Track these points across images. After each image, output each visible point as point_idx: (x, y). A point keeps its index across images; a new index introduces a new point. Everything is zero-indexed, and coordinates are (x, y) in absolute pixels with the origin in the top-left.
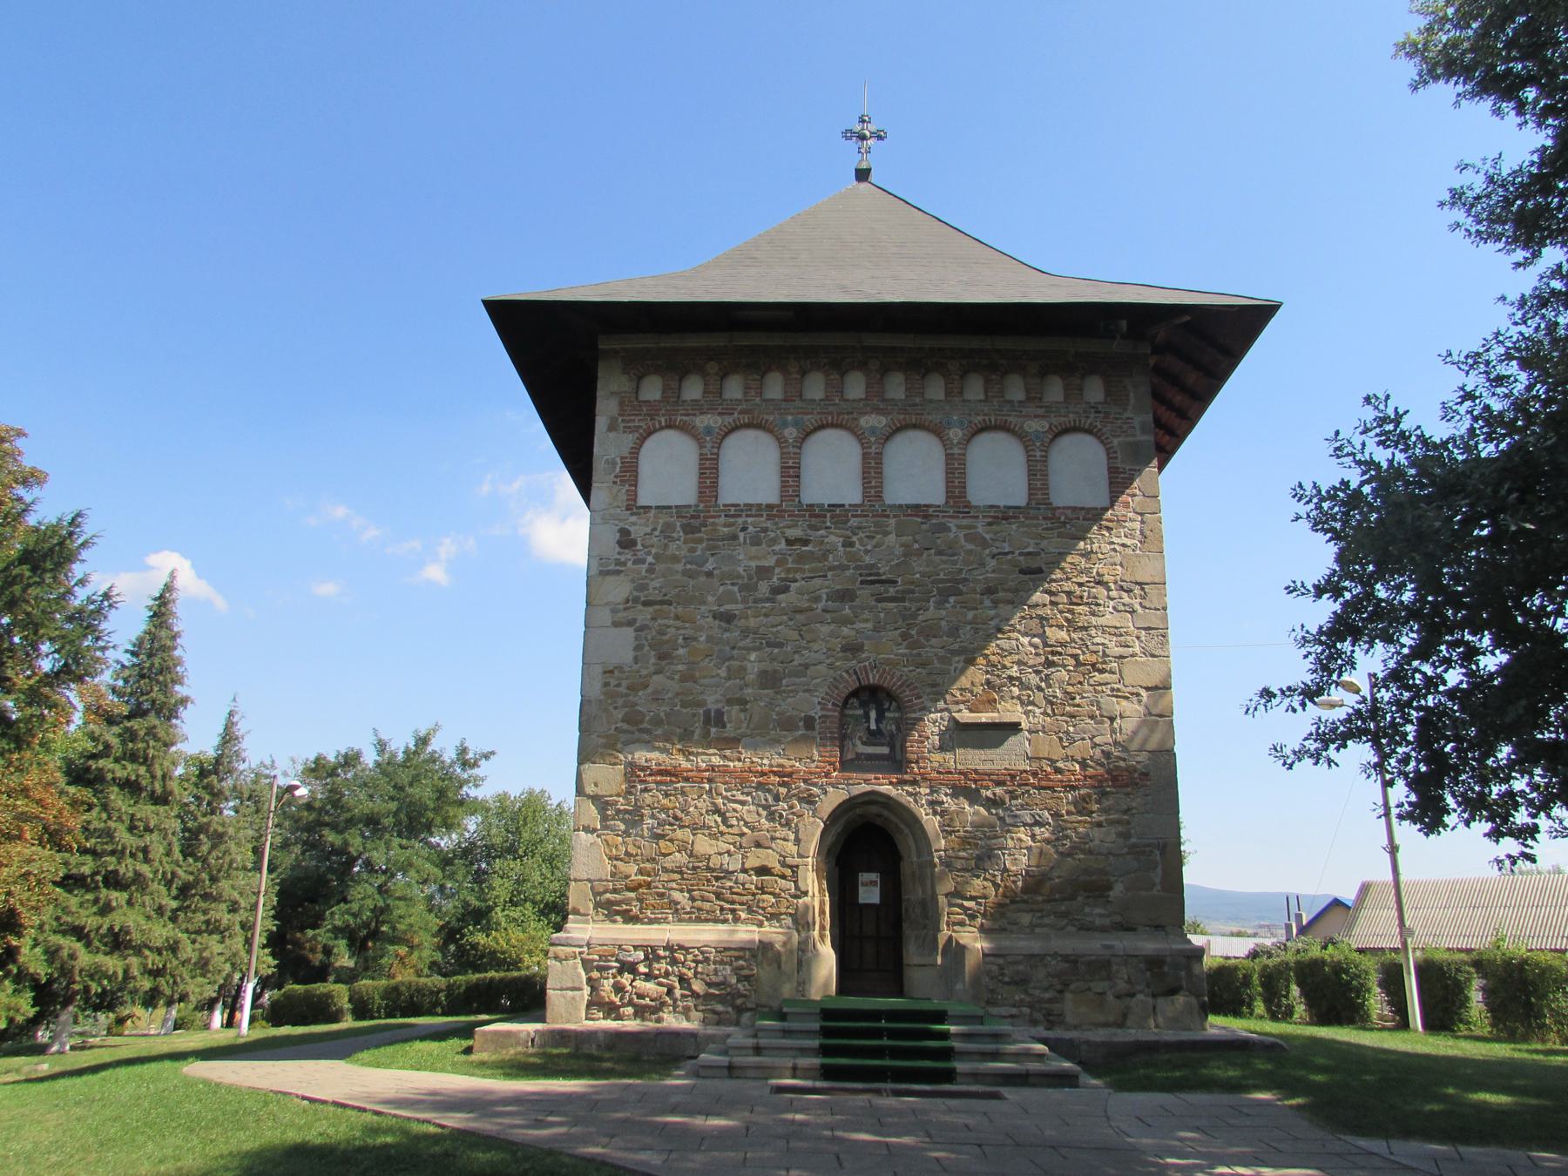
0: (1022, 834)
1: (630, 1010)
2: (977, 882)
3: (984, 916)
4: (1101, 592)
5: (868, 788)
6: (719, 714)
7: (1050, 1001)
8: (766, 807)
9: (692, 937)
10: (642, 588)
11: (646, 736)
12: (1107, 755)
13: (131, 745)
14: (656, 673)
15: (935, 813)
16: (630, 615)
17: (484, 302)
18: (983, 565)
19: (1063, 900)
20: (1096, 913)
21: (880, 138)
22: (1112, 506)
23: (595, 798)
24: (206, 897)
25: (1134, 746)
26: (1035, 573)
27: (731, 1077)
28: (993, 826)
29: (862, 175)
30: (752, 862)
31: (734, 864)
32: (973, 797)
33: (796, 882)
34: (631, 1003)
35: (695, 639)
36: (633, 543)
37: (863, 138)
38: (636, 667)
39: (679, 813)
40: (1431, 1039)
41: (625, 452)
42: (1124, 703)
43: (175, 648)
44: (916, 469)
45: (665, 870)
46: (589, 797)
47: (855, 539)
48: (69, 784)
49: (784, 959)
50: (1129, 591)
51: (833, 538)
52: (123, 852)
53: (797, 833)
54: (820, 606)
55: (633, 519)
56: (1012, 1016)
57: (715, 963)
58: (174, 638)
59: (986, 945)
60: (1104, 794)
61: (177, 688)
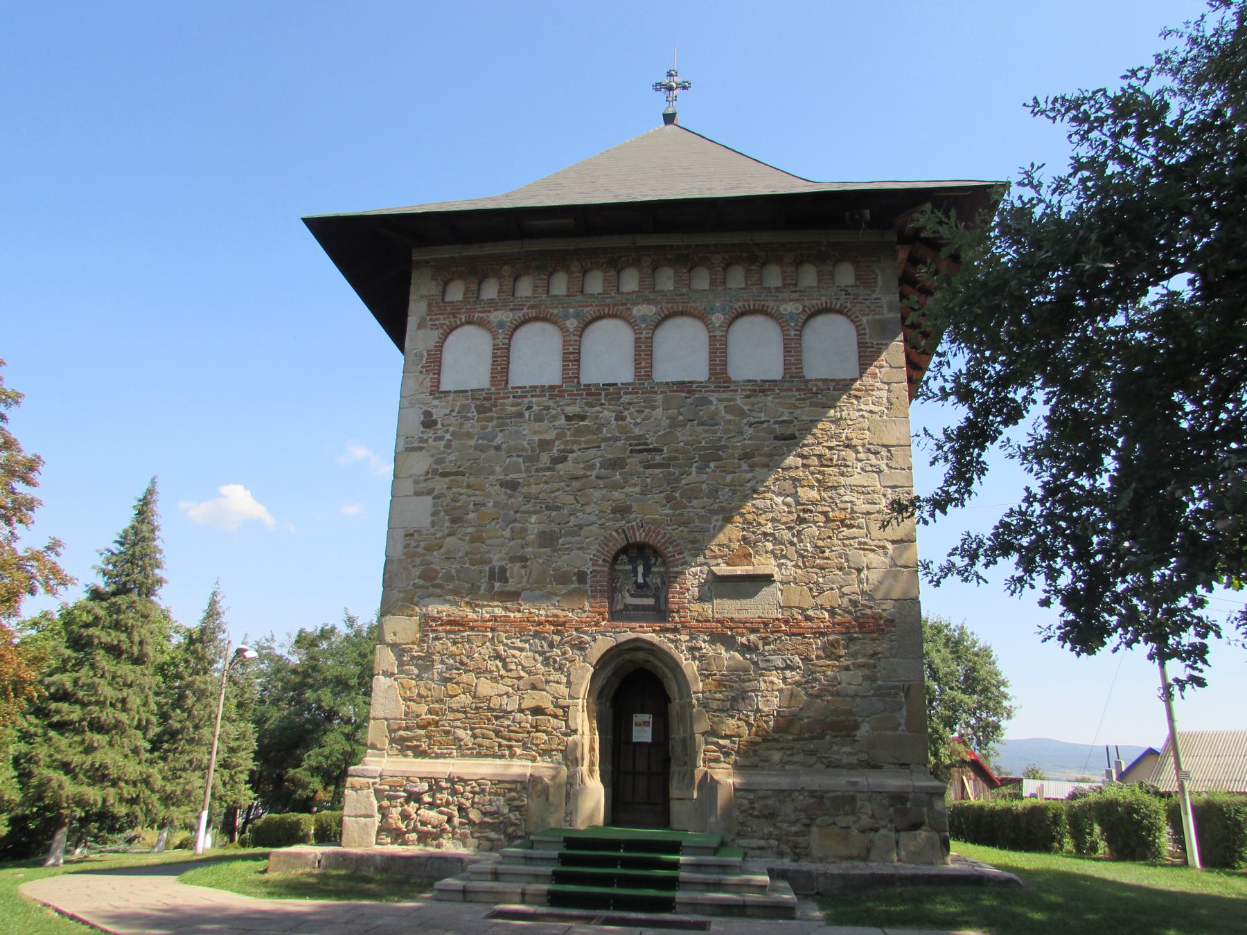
0: (775, 677)
1: (414, 836)
2: (732, 722)
3: (738, 753)
4: (850, 455)
5: (634, 635)
6: (503, 570)
7: (796, 834)
8: (542, 653)
9: (471, 770)
10: (440, 461)
11: (438, 591)
12: (854, 603)
13: (115, 616)
14: (449, 535)
15: (694, 658)
16: (430, 485)
17: (309, 222)
18: (741, 433)
19: (812, 738)
20: (843, 752)
21: (685, 88)
22: (862, 371)
23: (393, 646)
24: (191, 741)
25: (879, 595)
26: (789, 439)
27: (465, 901)
28: (746, 670)
29: (669, 119)
30: (529, 703)
31: (512, 705)
32: (729, 643)
33: (566, 721)
34: (415, 830)
35: (484, 505)
36: (435, 423)
37: (670, 89)
38: (432, 530)
39: (465, 659)
40: (1207, 876)
41: (431, 345)
42: (871, 555)
43: (154, 539)
44: (682, 352)
45: (452, 710)
46: (388, 645)
47: (626, 413)
48: (67, 648)
49: (551, 790)
50: (876, 453)
51: (606, 413)
52: (104, 703)
53: (568, 676)
54: (594, 473)
55: (436, 402)
56: (761, 848)
57: (490, 794)
58: (153, 531)
59: (737, 780)
60: (852, 640)
61: (157, 571)
